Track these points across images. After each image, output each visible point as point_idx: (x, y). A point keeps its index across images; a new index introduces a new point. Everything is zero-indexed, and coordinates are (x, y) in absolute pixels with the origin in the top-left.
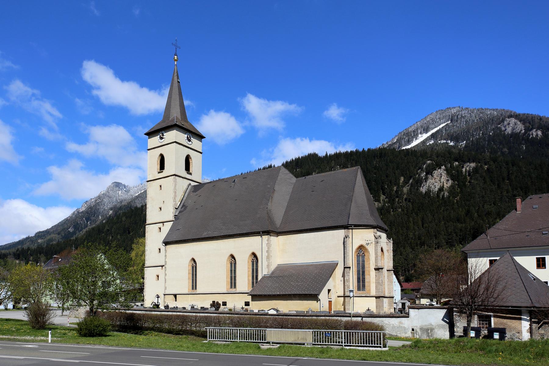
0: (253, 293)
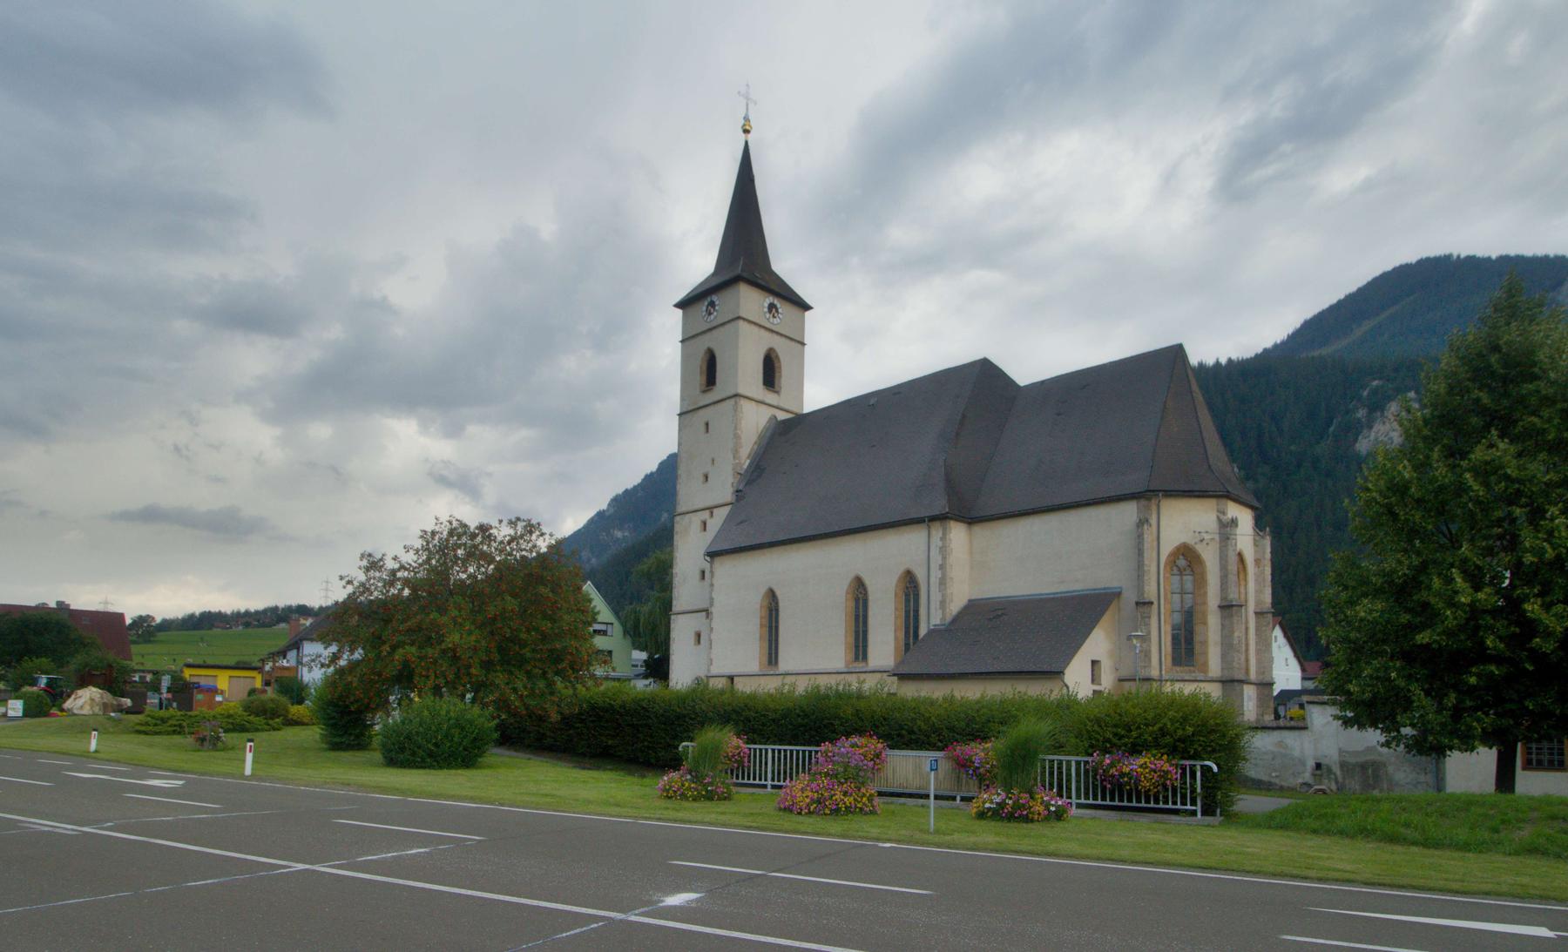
0: (901, 671)
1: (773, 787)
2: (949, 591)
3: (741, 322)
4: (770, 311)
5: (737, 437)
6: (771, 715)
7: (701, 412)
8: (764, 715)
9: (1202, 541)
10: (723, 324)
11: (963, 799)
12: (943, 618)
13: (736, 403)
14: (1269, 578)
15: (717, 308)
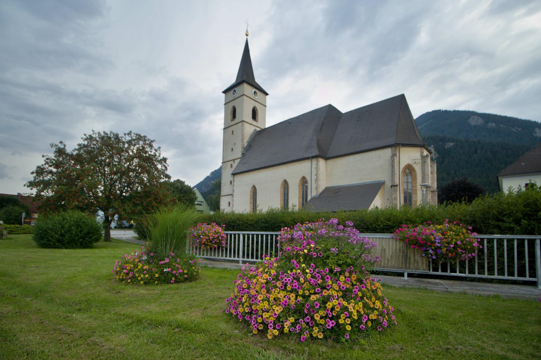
1: (244, 262)
2: (319, 184)
3: (244, 97)
4: (255, 94)
5: (243, 135)
8: (246, 223)
9: (415, 163)
10: (238, 97)
11: (410, 275)
12: (317, 193)
13: (242, 124)
14: (436, 179)
15: (236, 92)
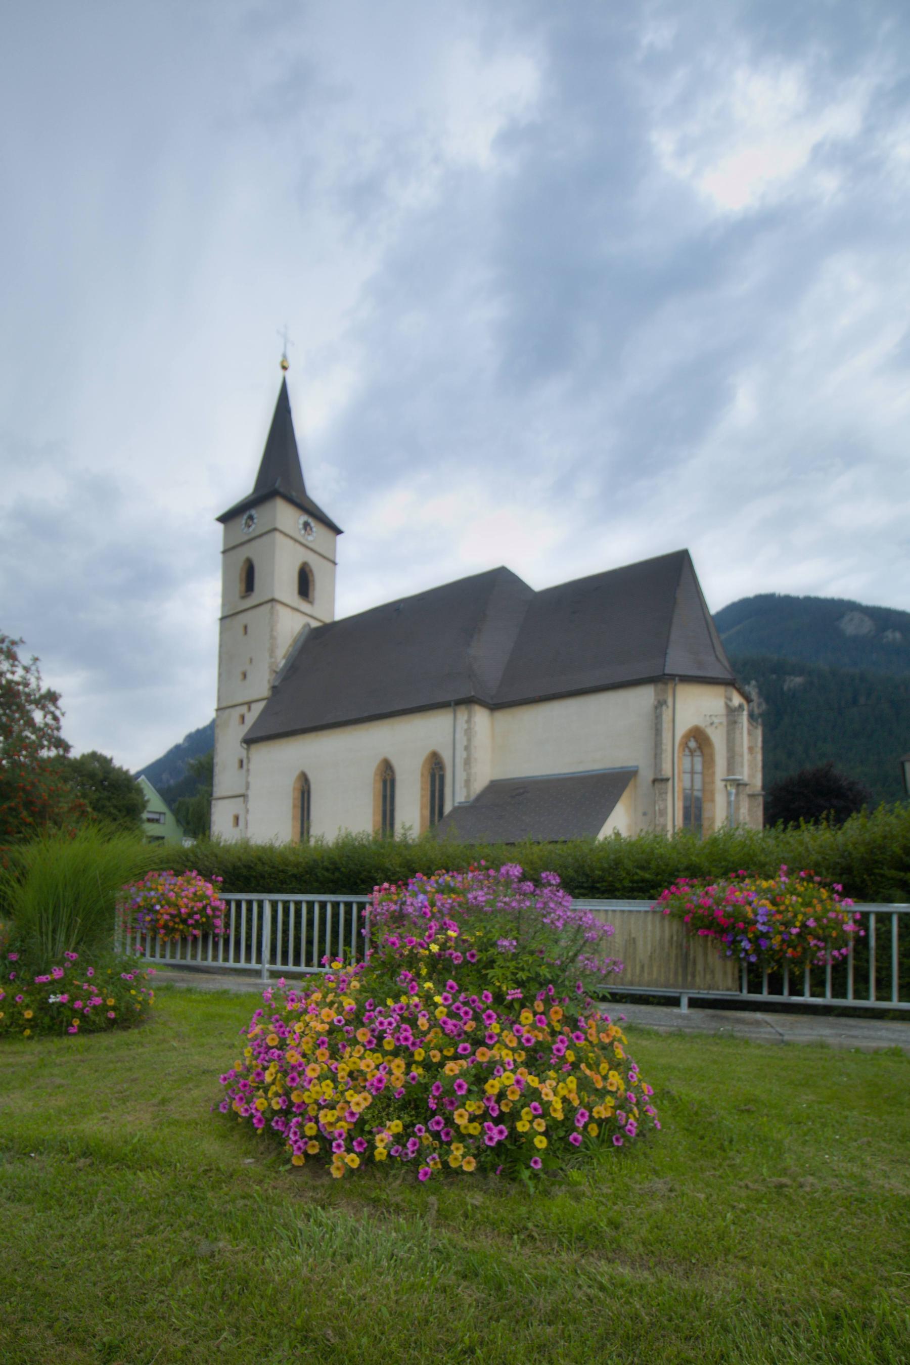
1: (274, 974)
5: (273, 638)
6: (292, 870)
7: (241, 616)
8: (283, 871)
9: (712, 724)
10: (261, 536)
11: (694, 1003)
12: (468, 796)
13: (272, 607)
